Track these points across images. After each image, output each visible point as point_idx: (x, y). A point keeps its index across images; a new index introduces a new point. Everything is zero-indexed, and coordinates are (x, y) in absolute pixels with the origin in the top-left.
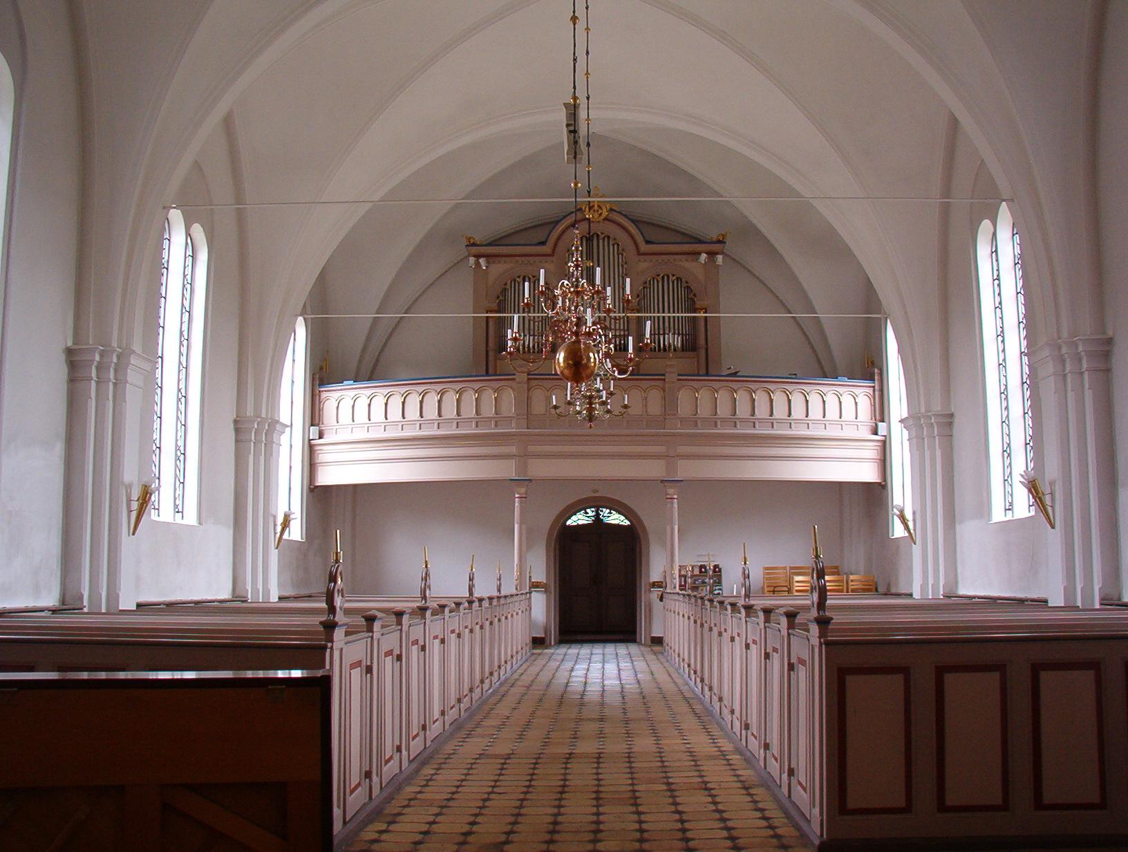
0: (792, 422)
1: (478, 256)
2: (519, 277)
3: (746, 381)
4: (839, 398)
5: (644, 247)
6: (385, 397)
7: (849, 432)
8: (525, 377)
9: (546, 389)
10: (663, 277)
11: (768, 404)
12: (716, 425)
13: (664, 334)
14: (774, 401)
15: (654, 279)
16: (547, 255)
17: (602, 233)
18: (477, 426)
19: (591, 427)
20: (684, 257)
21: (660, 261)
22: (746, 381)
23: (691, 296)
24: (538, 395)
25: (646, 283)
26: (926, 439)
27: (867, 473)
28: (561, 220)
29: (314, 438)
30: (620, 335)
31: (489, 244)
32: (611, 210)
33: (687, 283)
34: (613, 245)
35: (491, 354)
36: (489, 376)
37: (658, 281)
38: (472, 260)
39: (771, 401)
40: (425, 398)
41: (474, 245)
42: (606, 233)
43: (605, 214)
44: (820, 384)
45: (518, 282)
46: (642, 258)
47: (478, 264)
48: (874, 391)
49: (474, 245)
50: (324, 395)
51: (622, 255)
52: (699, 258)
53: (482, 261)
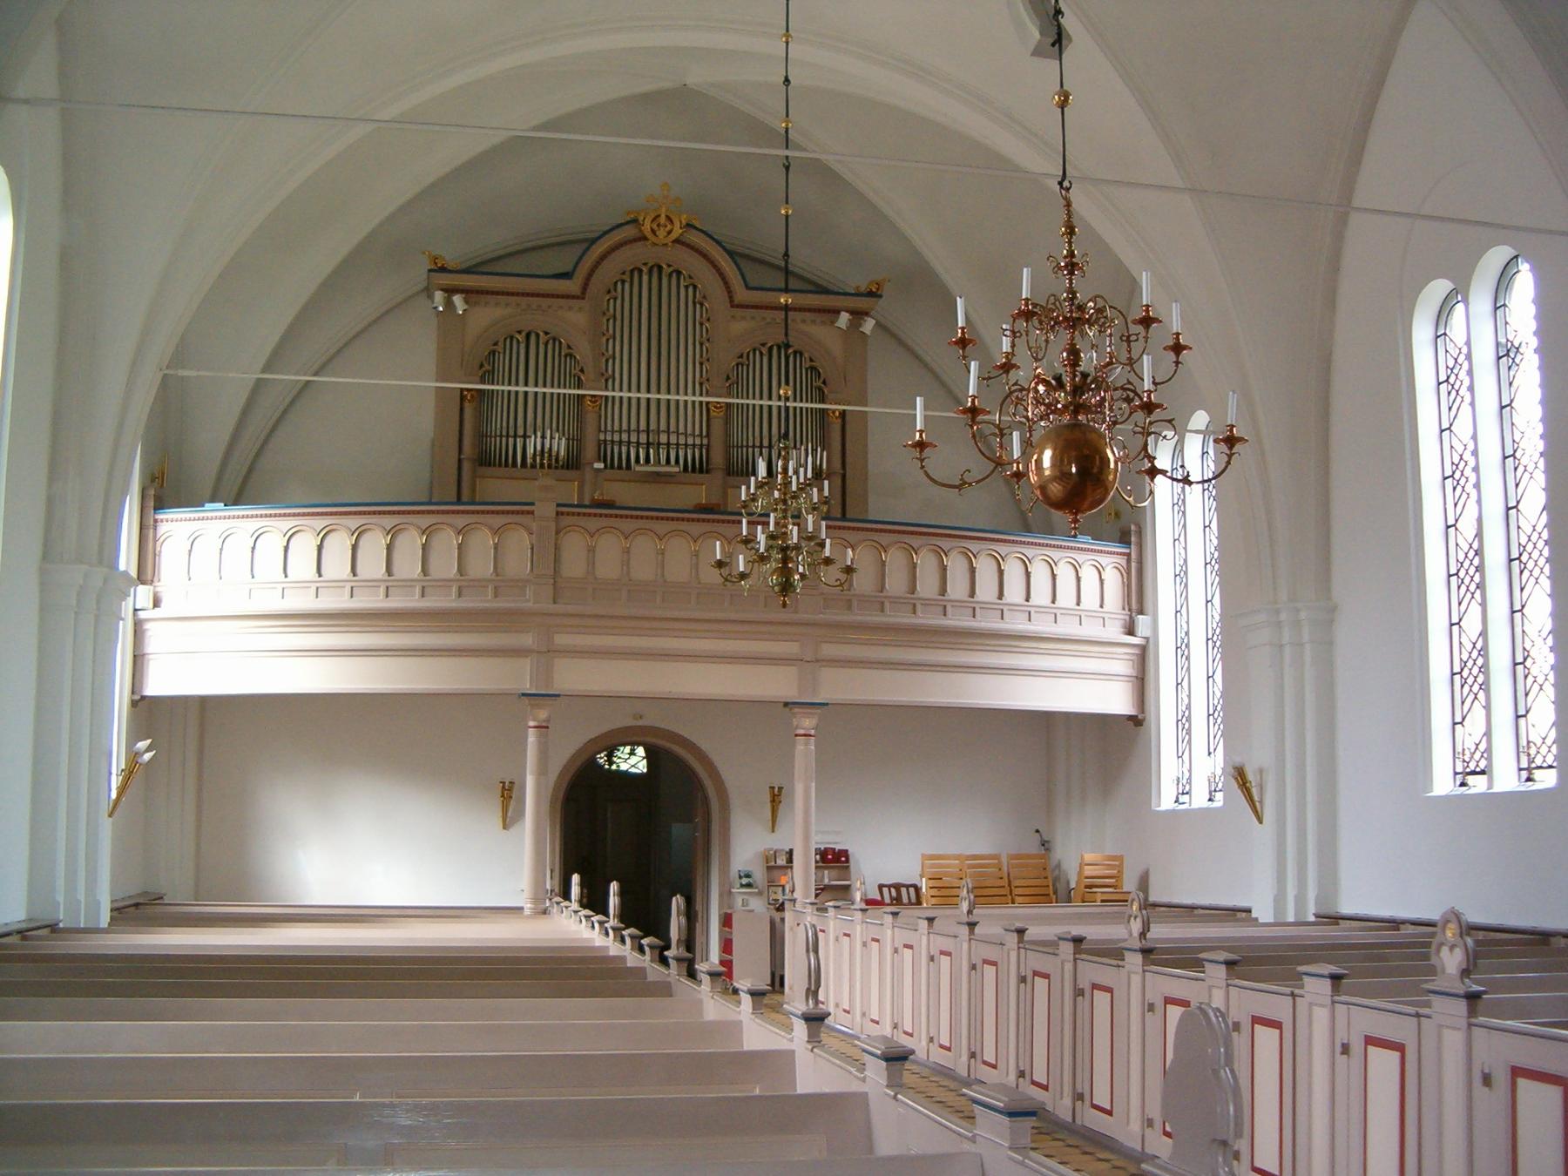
0: (1083, 614)
1: (450, 291)
2: (520, 332)
3: (904, 532)
4: (1077, 571)
5: (742, 294)
6: (318, 535)
7: (1091, 630)
8: (551, 510)
9: (623, 533)
10: (770, 349)
11: (967, 576)
12: (850, 607)
13: (525, 436)
14: (1032, 575)
15: (754, 350)
16: (574, 297)
17: (669, 266)
18: (460, 595)
19: (784, 605)
20: (808, 315)
21: (768, 320)
22: (904, 532)
23: (819, 383)
24: (574, 546)
25: (741, 356)
26: (1308, 647)
27: (1115, 700)
28: (600, 237)
29: (145, 606)
30: (694, 445)
31: (467, 271)
32: (689, 226)
33: (811, 360)
34: (687, 287)
35: (466, 466)
36: (464, 504)
37: (761, 354)
38: (439, 296)
39: (944, 569)
40: (361, 543)
41: (443, 269)
42: (676, 267)
43: (677, 232)
44: (1050, 546)
45: (518, 340)
46: (739, 312)
47: (449, 304)
48: (1129, 561)
49: (443, 269)
50: (163, 529)
51: (702, 305)
52: (860, 325)
53: (458, 300)
